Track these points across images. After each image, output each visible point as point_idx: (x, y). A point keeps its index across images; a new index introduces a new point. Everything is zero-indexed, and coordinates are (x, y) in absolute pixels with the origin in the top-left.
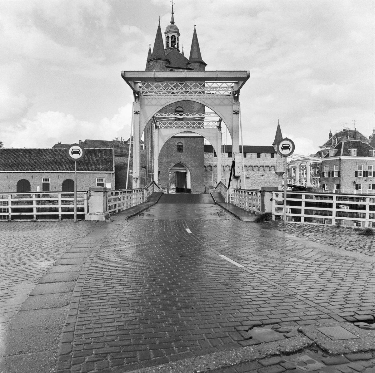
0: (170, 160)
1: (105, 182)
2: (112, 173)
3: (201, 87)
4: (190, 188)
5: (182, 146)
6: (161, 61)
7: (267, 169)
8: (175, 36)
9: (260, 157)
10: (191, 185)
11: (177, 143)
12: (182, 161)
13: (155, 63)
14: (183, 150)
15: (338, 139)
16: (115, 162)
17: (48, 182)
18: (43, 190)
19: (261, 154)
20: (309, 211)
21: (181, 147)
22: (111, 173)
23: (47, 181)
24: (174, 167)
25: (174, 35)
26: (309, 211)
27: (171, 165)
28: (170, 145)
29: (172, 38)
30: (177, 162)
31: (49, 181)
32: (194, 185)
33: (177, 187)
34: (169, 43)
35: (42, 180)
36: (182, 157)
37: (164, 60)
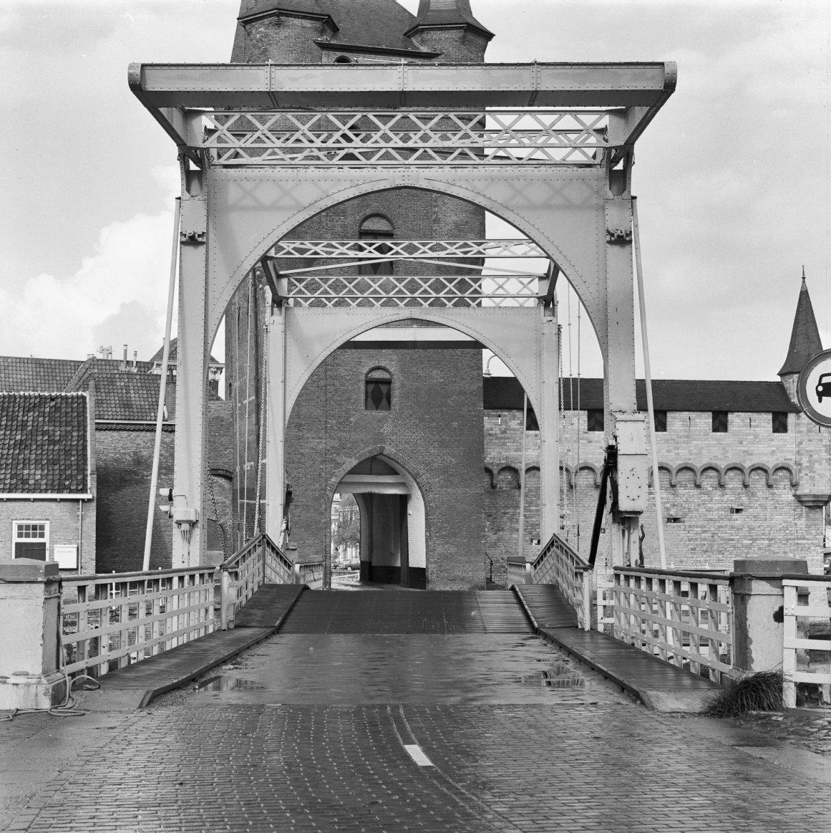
1: (53, 542)
2: (83, 500)
5: (388, 382)
6: (297, 21)
7: (758, 481)
10: (429, 551)
11: (365, 370)
12: (389, 449)
13: (271, 31)
14: (394, 400)
17: (38, 540)
19: (730, 416)
21: (384, 388)
22: (77, 501)
23: (34, 536)
27: (338, 465)
30: (366, 451)
31: (42, 535)
35: (15, 531)
36: (387, 429)
37: (311, 19)
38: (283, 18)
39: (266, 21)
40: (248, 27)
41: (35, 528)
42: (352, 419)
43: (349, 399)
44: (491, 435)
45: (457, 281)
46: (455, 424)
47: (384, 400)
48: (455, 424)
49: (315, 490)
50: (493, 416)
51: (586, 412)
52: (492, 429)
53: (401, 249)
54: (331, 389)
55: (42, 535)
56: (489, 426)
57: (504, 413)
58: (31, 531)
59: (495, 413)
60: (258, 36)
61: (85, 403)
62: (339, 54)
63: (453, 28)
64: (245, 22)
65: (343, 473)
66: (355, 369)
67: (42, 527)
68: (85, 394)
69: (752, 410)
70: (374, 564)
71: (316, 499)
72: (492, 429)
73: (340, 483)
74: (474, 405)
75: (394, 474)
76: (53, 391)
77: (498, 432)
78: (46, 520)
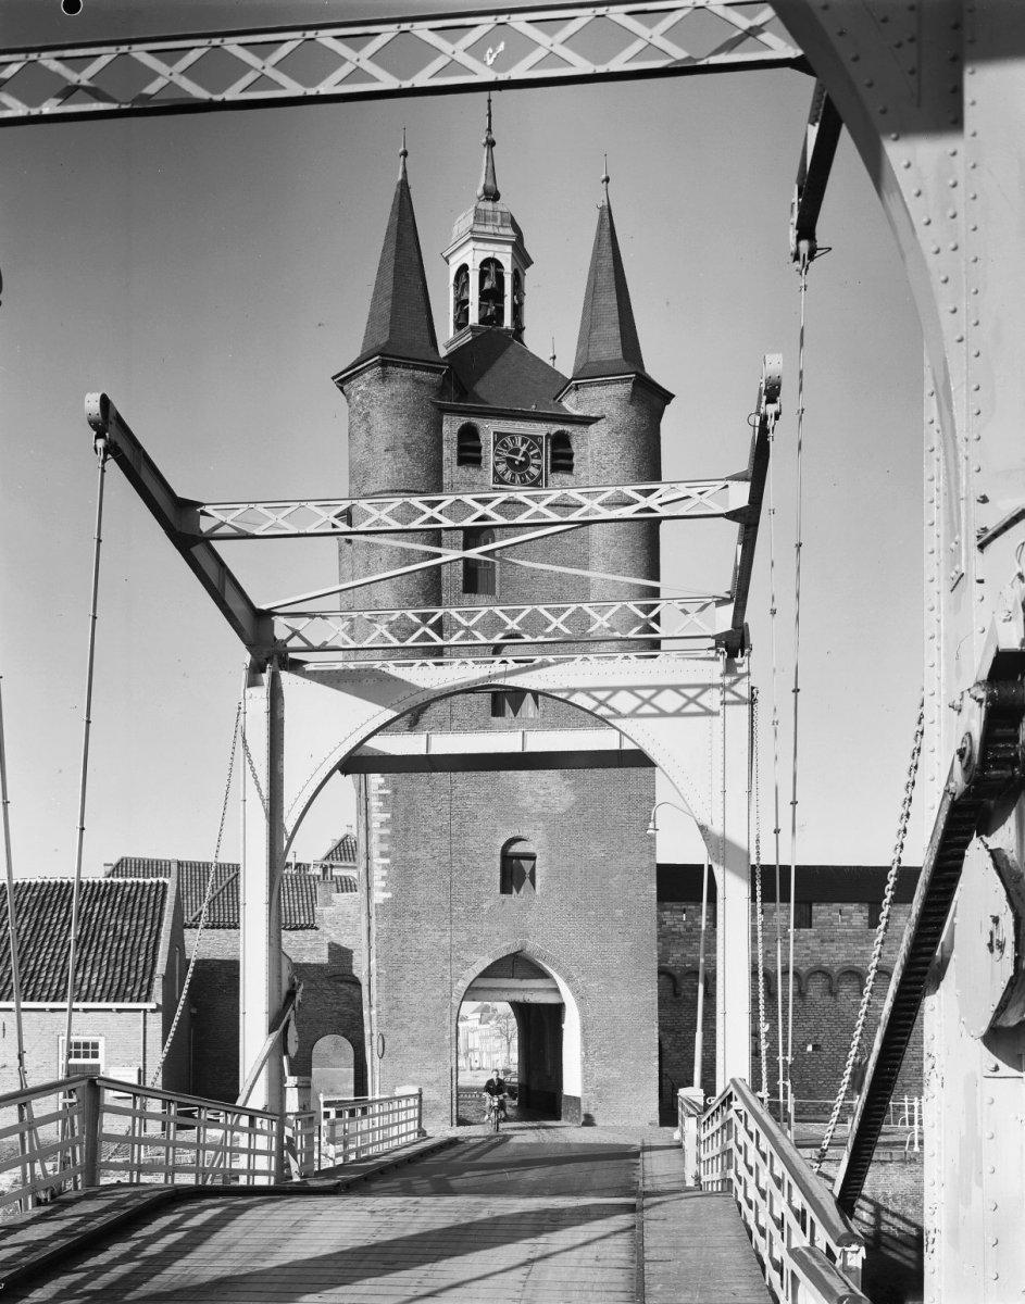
0: (463, 936)
3: (271, 73)
4: (577, 1093)
8: (499, 265)
9: (569, 468)
10: (587, 1076)
11: (502, 842)
14: (538, 881)
15: (225, 1164)
16: (789, 908)
18: (165, 1085)
20: (931, 929)
23: (86, 1056)
24: (485, 974)
25: (498, 257)
26: (931, 929)
27: (467, 965)
28: (463, 852)
29: (483, 276)
30: (503, 948)
31: (95, 1055)
32: (598, 1075)
33: (525, 1082)
34: (467, 302)
38: (390, 368)
39: (367, 376)
40: (345, 387)
41: (86, 1045)
42: (485, 906)
43: (480, 880)
44: (673, 933)
45: (568, 612)
46: (619, 912)
47: (528, 881)
48: (619, 912)
49: (437, 997)
50: (676, 910)
52: (674, 926)
53: (440, 512)
54: (457, 866)
55: (95, 1055)
56: (671, 923)
57: (690, 907)
58: (82, 1050)
59: (678, 907)
60: (358, 398)
61: (164, 892)
62: (465, 420)
63: (617, 381)
64: (342, 381)
65: (473, 976)
66: (488, 841)
67: (95, 1046)
68: (167, 881)
69: (1013, 896)
70: (534, 1087)
71: (439, 1008)
72: (674, 926)
73: (469, 988)
74: (644, 886)
75: (542, 978)
76: (148, 877)
77: (682, 929)
78: (101, 1035)
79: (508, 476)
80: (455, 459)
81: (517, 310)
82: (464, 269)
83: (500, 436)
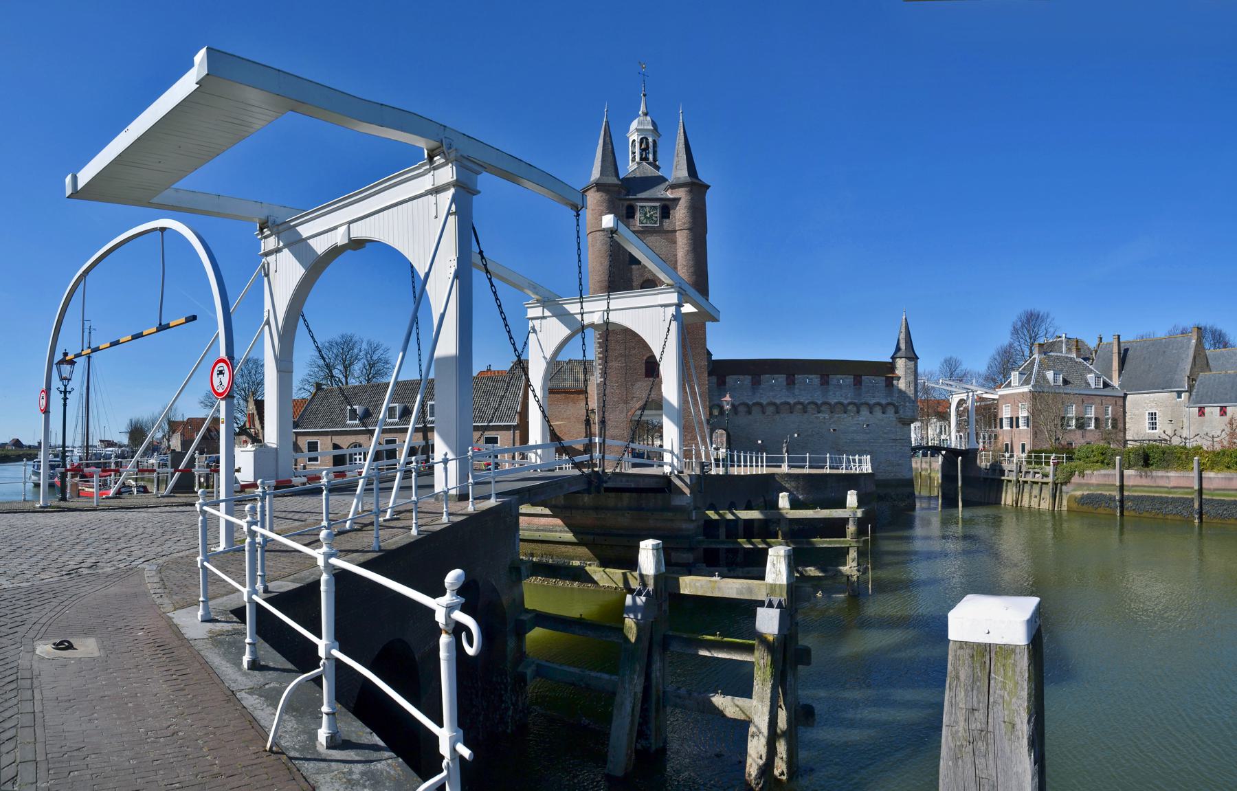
29: (641, 142)
51: (785, 375)
79: (645, 221)
80: (625, 217)
81: (655, 153)
82: (634, 141)
83: (642, 207)
